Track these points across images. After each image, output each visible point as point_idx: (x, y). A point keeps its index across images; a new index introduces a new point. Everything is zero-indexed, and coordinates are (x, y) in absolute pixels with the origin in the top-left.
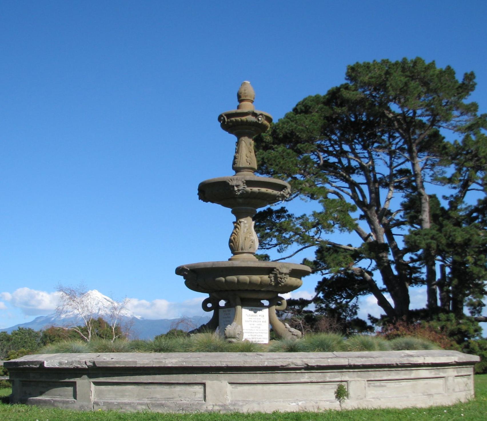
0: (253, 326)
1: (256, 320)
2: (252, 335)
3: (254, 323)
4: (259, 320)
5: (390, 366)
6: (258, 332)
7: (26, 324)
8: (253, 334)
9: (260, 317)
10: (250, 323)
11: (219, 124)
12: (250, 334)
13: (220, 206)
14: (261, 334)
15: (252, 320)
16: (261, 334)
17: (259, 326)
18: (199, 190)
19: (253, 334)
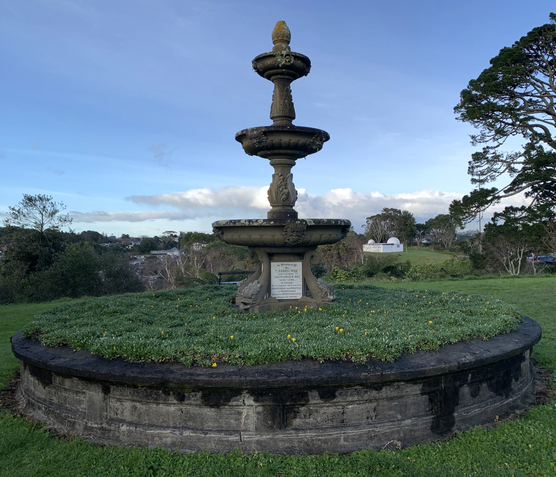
1: (288, 275)
6: (290, 287)
9: (293, 272)
10: (280, 279)
12: (280, 290)
14: (294, 290)
15: (283, 276)
16: (294, 290)
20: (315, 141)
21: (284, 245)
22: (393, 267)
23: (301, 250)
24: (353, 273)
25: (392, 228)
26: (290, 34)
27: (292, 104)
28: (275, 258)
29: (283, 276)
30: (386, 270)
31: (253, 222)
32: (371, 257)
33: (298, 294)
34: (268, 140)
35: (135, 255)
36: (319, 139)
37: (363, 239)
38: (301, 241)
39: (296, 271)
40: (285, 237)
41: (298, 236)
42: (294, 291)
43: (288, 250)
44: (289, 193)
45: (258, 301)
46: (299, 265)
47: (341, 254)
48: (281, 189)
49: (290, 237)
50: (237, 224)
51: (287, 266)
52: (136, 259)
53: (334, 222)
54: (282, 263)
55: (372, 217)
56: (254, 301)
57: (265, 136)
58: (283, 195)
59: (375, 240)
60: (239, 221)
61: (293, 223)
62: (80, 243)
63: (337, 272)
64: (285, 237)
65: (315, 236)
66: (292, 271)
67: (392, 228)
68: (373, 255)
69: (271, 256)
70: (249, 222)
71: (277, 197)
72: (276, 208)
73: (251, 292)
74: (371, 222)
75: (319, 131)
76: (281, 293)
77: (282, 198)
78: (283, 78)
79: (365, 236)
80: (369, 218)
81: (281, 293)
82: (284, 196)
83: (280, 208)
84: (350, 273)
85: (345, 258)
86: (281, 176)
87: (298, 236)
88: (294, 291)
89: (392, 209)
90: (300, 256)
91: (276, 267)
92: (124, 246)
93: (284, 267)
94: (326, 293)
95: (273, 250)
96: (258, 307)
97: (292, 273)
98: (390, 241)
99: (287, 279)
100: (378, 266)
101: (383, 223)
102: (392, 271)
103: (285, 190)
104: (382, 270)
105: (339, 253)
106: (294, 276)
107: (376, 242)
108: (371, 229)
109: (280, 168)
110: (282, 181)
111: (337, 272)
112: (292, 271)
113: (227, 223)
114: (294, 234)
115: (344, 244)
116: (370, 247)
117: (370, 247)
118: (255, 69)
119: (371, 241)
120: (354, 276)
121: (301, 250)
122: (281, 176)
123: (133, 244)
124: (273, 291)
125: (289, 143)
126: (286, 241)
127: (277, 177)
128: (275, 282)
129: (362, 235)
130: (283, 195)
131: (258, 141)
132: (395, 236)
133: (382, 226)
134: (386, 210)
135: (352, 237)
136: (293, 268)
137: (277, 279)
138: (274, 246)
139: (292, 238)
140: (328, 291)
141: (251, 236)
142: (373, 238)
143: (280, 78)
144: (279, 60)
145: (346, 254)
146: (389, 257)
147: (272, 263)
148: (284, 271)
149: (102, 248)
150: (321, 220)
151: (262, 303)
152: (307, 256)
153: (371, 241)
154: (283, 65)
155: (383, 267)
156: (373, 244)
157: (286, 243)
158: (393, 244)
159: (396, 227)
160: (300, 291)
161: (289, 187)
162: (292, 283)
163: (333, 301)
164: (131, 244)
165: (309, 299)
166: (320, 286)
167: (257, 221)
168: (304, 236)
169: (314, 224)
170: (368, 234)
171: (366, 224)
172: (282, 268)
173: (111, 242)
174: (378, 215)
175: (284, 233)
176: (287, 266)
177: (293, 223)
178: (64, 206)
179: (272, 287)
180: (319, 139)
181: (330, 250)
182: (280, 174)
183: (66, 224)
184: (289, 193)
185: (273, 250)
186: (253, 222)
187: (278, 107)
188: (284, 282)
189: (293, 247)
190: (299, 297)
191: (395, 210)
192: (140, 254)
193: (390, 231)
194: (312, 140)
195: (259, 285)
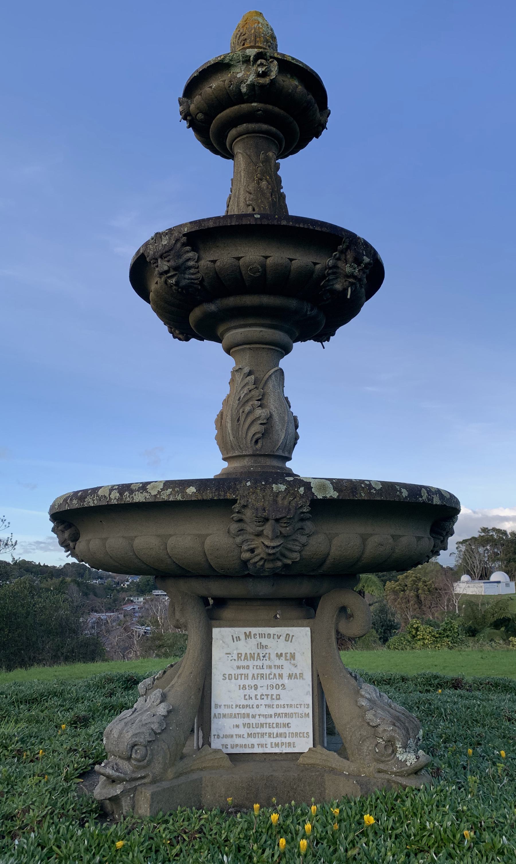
0: (253, 693)
1: (266, 671)
2: (248, 725)
3: (259, 682)
4: (277, 671)
5: (198, 739)
6: (271, 711)
7: (306, 478)
8: (252, 721)
9: (282, 662)
10: (242, 682)
11: (185, 123)
12: (239, 721)
13: (165, 328)
14: (286, 720)
15: (250, 672)
16: (286, 720)
17: (275, 692)
18: (302, 144)
19: (252, 721)
20: (340, 264)
21: (243, 572)
22: (509, 620)
23: (303, 589)
24: (445, 630)
25: (495, 557)
26: (273, 38)
27: (282, 197)
28: (227, 613)
29: (250, 672)
30: (497, 625)
31: (132, 492)
32: (471, 602)
33: (298, 735)
34: (202, 263)
35: (131, 596)
36: (350, 256)
37: (454, 575)
38: (296, 556)
39: (293, 656)
40: (239, 540)
41: (285, 537)
42: (288, 725)
43: (263, 588)
44: (270, 418)
45: (157, 768)
46: (302, 635)
47: (422, 597)
48: (247, 408)
49: (256, 542)
50: (90, 502)
51: (264, 641)
52: (132, 601)
53: (405, 493)
54: (247, 630)
55: (465, 541)
56: (138, 768)
57: (195, 249)
58: (261, 434)
59: (471, 575)
60: (95, 490)
61: (263, 490)
62: (61, 579)
63: (417, 629)
64: (239, 540)
65: (343, 539)
66: (279, 656)
67: (495, 557)
68: (473, 600)
69: (215, 610)
70: (121, 494)
71: (236, 431)
72: (237, 464)
73: (128, 737)
74: (463, 548)
75: (353, 240)
76: (242, 731)
77: (250, 435)
78: (254, 132)
79: (455, 569)
80: (460, 543)
81: (242, 731)
82: (257, 428)
83: (246, 462)
84: (440, 630)
85: (428, 603)
86: (250, 373)
87: (285, 537)
88: (288, 725)
89: (494, 529)
90: (305, 607)
91: (231, 645)
92: (118, 584)
93: (253, 642)
94: (390, 742)
95: (217, 589)
96: (153, 788)
97: (278, 662)
98: (494, 577)
99: (263, 688)
100: (484, 617)
101: (481, 550)
102: (506, 626)
103: (259, 412)
104: (491, 624)
105: (418, 596)
106: (285, 672)
107: (473, 579)
108: (464, 560)
109: (247, 355)
110: (251, 387)
111: (417, 629)
112: (279, 656)
113: (65, 500)
114: (268, 529)
115: (425, 582)
116: (466, 587)
117: (466, 587)
118: (185, 118)
119: (465, 578)
120: (448, 636)
121: (303, 589)
122: (250, 373)
123: (130, 581)
124: (216, 725)
125: (264, 266)
126: (246, 555)
127: (239, 377)
128: (225, 693)
129: (451, 569)
130: (261, 434)
131: (172, 263)
132: (500, 569)
133: (480, 554)
134: (484, 530)
135: (437, 571)
136: (282, 647)
137: (233, 685)
138: (207, 572)
139: (262, 545)
140: (398, 736)
141: (132, 539)
142: (468, 573)
143: (248, 132)
144: (239, 75)
145: (430, 597)
146: (502, 602)
147: (216, 632)
148: (252, 657)
149: (87, 586)
150: (363, 481)
151: (170, 774)
152: (327, 610)
153: (465, 578)
154: (252, 86)
155: (492, 620)
156: (467, 582)
157: (245, 563)
158: (499, 582)
159: (502, 556)
160: (307, 726)
161: (272, 403)
162: (278, 697)
163: (416, 772)
164: (127, 581)
165: (333, 759)
166: (369, 716)
167: (144, 487)
168: (303, 539)
169: (335, 495)
170: (459, 567)
171: (456, 551)
172: (247, 647)
173: (101, 578)
174: (473, 538)
175: (234, 527)
176: (264, 641)
177: (263, 490)
178: (6, 523)
179: (214, 711)
180: (350, 256)
181: (404, 591)
182: (246, 370)
183: (8, 550)
184: (270, 418)
185: (217, 589)
186: (132, 492)
187: (242, 199)
188: (253, 693)
189: (276, 576)
190: (304, 745)
191: (499, 531)
192: (139, 595)
193: (494, 561)
194: (331, 262)
195: (162, 710)
